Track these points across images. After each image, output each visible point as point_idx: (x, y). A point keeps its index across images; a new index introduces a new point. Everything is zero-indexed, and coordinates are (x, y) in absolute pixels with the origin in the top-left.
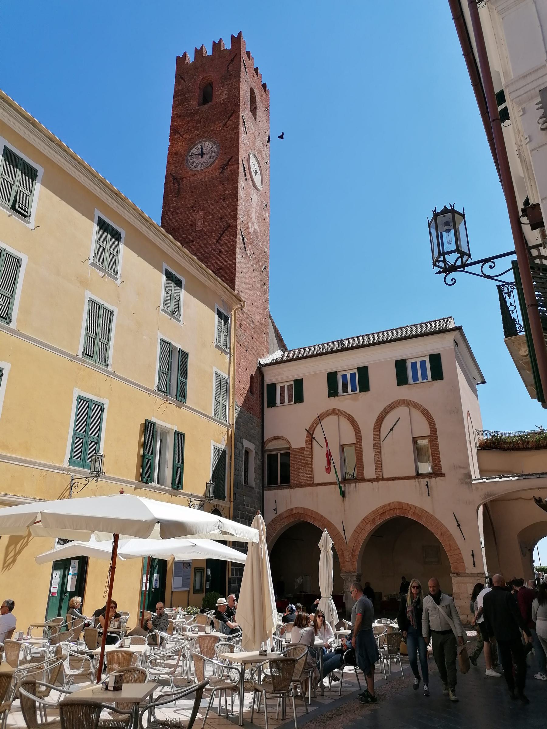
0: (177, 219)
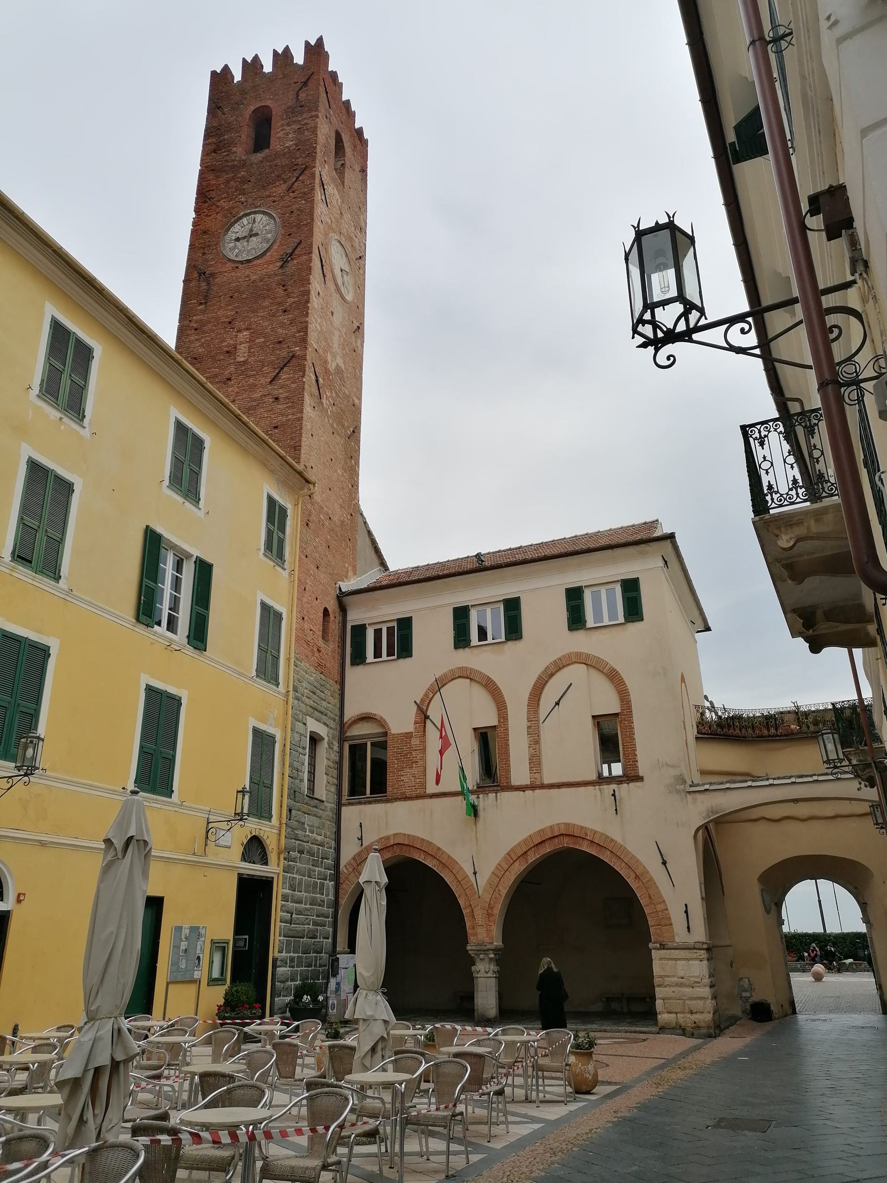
0: (203, 340)
